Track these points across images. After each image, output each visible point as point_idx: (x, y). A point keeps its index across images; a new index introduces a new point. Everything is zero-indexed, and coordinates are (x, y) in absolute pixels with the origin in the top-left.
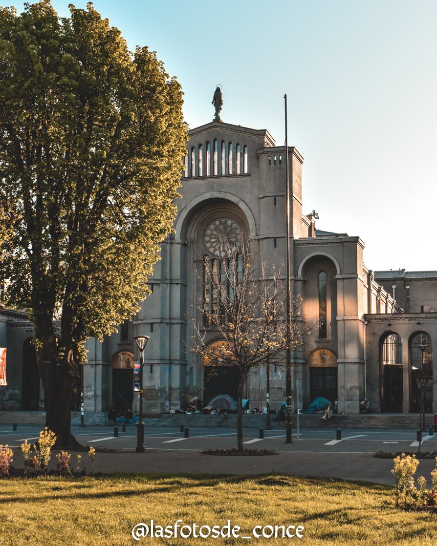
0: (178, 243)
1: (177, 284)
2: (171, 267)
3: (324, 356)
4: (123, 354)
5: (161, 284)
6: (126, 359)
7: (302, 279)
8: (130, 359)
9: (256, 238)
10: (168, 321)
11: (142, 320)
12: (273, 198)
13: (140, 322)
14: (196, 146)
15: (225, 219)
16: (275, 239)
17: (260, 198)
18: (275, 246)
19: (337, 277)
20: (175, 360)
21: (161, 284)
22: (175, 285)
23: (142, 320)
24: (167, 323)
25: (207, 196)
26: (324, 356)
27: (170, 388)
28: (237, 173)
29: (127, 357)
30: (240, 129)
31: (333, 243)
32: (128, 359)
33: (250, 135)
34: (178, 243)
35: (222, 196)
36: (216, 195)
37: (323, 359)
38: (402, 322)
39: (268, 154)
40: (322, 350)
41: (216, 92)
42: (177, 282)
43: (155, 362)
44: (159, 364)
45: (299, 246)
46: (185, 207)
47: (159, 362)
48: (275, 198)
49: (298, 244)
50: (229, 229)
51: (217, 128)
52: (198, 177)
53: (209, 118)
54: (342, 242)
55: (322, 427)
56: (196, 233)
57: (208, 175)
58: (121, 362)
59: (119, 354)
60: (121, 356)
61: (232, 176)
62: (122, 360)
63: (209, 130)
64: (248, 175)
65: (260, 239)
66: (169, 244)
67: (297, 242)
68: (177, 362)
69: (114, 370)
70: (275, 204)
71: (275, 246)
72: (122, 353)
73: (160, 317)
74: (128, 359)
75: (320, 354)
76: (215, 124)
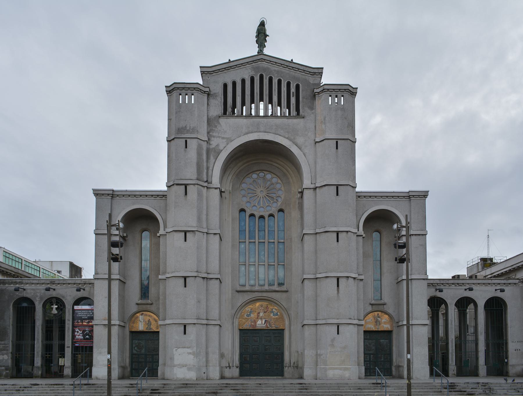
0: (216, 188)
2: (207, 215)
3: (379, 319)
4: (142, 314)
6: (147, 320)
8: (151, 320)
9: (313, 186)
10: (205, 275)
12: (335, 141)
15: (264, 172)
16: (337, 186)
17: (316, 142)
18: (337, 195)
21: (196, 232)
22: (212, 235)
24: (204, 278)
26: (379, 319)
29: (148, 318)
32: (149, 321)
33: (303, 74)
34: (216, 188)
38: (448, 287)
40: (376, 313)
41: (259, 26)
48: (337, 142)
49: (359, 196)
50: (269, 183)
53: (253, 50)
55: (239, 378)
56: (231, 184)
58: (140, 324)
59: (138, 315)
60: (140, 316)
62: (141, 322)
63: (254, 64)
65: (317, 187)
69: (132, 332)
70: (337, 148)
71: (337, 195)
72: (141, 313)
73: (196, 270)
74: (149, 321)
75: (374, 317)
76: (259, 57)
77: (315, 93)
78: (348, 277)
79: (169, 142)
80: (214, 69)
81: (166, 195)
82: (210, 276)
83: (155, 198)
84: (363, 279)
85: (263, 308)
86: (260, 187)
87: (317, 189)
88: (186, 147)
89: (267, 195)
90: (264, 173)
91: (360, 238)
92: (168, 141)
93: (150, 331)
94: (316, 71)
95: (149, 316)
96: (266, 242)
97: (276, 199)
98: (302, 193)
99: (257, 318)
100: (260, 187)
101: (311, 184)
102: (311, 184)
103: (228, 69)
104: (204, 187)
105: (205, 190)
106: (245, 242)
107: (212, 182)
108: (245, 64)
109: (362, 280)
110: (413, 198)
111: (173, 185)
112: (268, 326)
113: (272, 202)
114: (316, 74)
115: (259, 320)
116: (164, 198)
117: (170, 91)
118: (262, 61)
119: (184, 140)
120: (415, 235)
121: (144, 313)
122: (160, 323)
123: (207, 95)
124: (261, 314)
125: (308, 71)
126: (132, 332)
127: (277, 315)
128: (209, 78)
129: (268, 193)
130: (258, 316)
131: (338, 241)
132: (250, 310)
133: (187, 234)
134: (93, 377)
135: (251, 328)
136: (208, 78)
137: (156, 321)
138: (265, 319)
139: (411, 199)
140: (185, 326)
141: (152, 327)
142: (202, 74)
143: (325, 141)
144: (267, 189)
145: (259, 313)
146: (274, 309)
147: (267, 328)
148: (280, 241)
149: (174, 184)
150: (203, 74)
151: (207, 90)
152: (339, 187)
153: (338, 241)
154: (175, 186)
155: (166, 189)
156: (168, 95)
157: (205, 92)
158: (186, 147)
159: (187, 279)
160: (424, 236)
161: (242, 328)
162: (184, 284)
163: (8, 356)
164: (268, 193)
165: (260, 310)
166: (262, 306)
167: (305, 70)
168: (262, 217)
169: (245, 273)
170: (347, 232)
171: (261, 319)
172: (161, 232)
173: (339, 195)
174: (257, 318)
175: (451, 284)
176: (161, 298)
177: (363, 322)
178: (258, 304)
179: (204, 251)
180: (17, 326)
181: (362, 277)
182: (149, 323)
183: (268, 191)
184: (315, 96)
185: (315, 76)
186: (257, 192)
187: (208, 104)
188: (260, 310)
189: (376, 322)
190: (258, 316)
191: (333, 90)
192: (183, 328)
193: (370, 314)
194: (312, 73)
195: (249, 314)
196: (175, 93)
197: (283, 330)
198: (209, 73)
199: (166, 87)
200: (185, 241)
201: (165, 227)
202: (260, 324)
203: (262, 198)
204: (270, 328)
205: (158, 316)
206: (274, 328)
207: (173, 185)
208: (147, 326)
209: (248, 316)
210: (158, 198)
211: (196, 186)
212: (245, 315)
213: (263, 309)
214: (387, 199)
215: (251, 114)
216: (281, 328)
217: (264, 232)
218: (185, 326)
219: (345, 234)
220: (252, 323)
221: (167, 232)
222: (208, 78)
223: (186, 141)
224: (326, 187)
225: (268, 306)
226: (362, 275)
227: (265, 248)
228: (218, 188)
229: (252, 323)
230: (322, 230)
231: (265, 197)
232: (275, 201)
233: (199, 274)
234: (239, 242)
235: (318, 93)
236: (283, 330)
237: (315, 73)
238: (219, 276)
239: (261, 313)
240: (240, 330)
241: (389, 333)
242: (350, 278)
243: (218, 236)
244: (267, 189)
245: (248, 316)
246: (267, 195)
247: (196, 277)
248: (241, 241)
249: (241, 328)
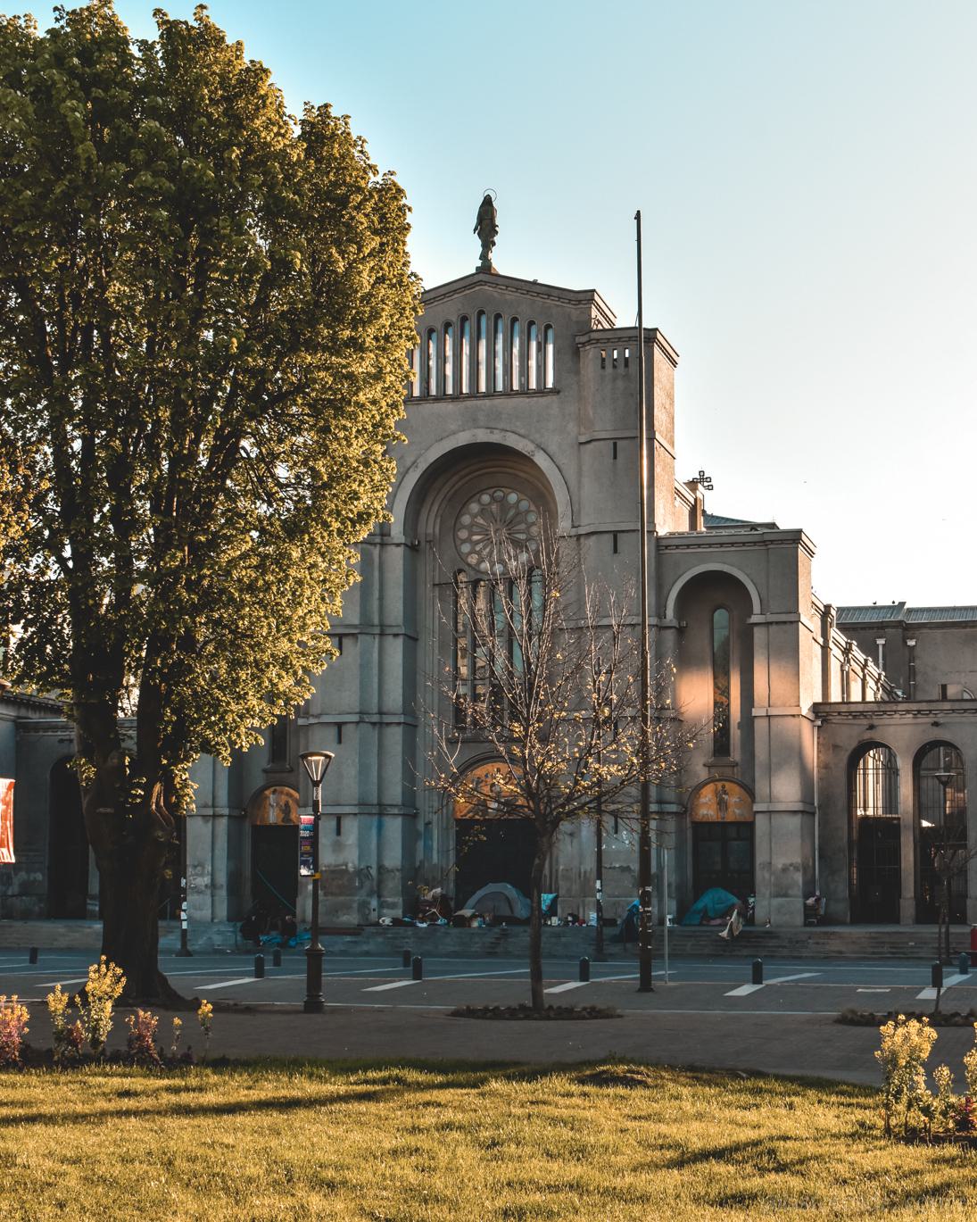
0: (398, 545)
2: (381, 598)
3: (726, 797)
6: (282, 803)
7: (675, 623)
8: (291, 802)
9: (573, 532)
10: (375, 719)
13: (312, 721)
14: (439, 326)
16: (615, 534)
17: (581, 443)
18: (615, 551)
19: (754, 619)
24: (374, 724)
25: (463, 439)
26: (726, 797)
27: (381, 868)
32: (287, 804)
34: (398, 545)
35: (495, 438)
36: (482, 436)
37: (722, 805)
40: (720, 785)
42: (395, 631)
43: (347, 810)
45: (668, 551)
48: (615, 444)
49: (667, 547)
51: (486, 288)
52: (442, 397)
59: (267, 792)
64: (555, 391)
67: (664, 543)
70: (615, 457)
71: (615, 551)
72: (272, 789)
74: (287, 804)
75: (716, 793)
94: (581, 297)
120: (777, 623)
121: (277, 788)
126: (256, 829)
159: (344, 729)
160: (794, 625)
163: (43, 875)
176: (735, 733)
179: (375, 671)
180: (273, 750)
189: (719, 804)
214: (733, 549)
215: (461, 393)
235: (583, 344)
237: (580, 301)
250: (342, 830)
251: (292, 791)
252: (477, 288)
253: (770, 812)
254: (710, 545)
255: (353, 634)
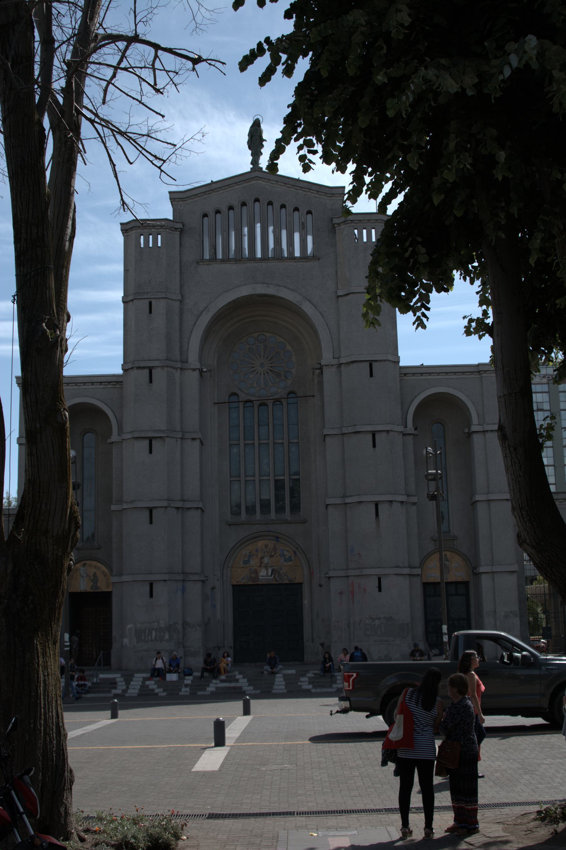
0: (194, 370)
1: (193, 439)
2: (181, 411)
5: (167, 439)
7: (413, 431)
9: (335, 362)
10: (179, 504)
11: (132, 502)
13: (125, 506)
14: (224, 209)
18: (371, 375)
19: (474, 428)
20: (191, 574)
21: (167, 439)
23: (132, 502)
24: (178, 508)
25: (245, 291)
27: (185, 624)
28: (205, 258)
30: (214, 186)
31: (101, 383)
32: (95, 575)
33: (317, 195)
34: (194, 370)
35: (271, 291)
36: (261, 289)
37: (443, 569)
39: (353, 224)
42: (193, 436)
43: (158, 577)
44: (165, 581)
45: (405, 378)
46: (206, 308)
47: (166, 577)
49: (405, 374)
51: (261, 182)
52: (226, 260)
54: (479, 372)
57: (270, 256)
60: (82, 568)
61: (287, 259)
62: (83, 577)
63: (245, 184)
64: (315, 257)
66: (179, 370)
67: (404, 371)
68: (196, 578)
71: (371, 375)
72: (83, 563)
74: (95, 575)
77: (334, 224)
78: (391, 502)
79: (126, 304)
80: (188, 194)
81: (122, 382)
82: (188, 505)
83: (105, 387)
84: (416, 503)
85: (268, 550)
86: (260, 357)
87: (343, 366)
88: (150, 312)
89: (270, 370)
90: (265, 336)
91: (410, 439)
92: (124, 302)
93: (96, 591)
95: (95, 567)
96: (270, 444)
97: (284, 376)
98: (321, 369)
99: (260, 566)
100: (260, 357)
101: (334, 358)
102: (334, 358)
103: (210, 194)
104: (176, 369)
105: (177, 374)
106: (239, 444)
107: (187, 359)
108: (232, 185)
109: (414, 504)
110: (485, 375)
111: (132, 368)
112: (278, 578)
113: (278, 380)
114: (336, 195)
115: (263, 570)
116: (117, 386)
117: (126, 230)
118: (257, 180)
119: (147, 302)
122: (115, 579)
123: (179, 233)
124: (266, 560)
125: (323, 191)
127: (291, 560)
128: (182, 207)
129: (271, 367)
130: (261, 563)
131: (374, 446)
132: (248, 554)
133: (154, 442)
134: (467, 580)
135: (250, 583)
136: (181, 207)
137: (105, 575)
138: (272, 567)
139: (483, 375)
140: (151, 585)
141: (99, 585)
142: (171, 202)
143: (350, 296)
144: (270, 360)
145: (262, 558)
146: (285, 552)
147: (275, 583)
148: (292, 441)
149: (134, 367)
150: (173, 201)
151: (179, 226)
152: (373, 364)
153: (374, 446)
154: (135, 371)
155: (121, 372)
156: (124, 235)
157: (176, 229)
158: (150, 312)
159: (154, 512)
161: (237, 582)
162: (148, 519)
164: (271, 367)
165: (264, 552)
166: (266, 546)
167: (318, 190)
168: (263, 404)
169: (239, 494)
170: (388, 432)
171: (266, 567)
172: (115, 437)
173: (374, 375)
174: (260, 566)
175: (563, 500)
177: (418, 571)
178: (260, 544)
181: (414, 499)
182: (95, 579)
183: (271, 363)
184: (334, 227)
185: (334, 198)
186: (254, 366)
187: (181, 245)
188: (264, 552)
190: (261, 563)
191: (359, 222)
192: (148, 588)
193: (433, 556)
194: (329, 194)
195: (246, 559)
196: (133, 233)
197: (301, 584)
198: (183, 200)
199: (121, 224)
200: (151, 452)
201: (121, 431)
202: (264, 575)
203: (262, 374)
204: (280, 582)
205: (110, 569)
206: (286, 582)
207: (132, 368)
208: (92, 583)
209: (246, 562)
210: (109, 386)
211: (166, 369)
212: (241, 563)
213: (269, 552)
216: (297, 581)
217: (267, 427)
218: (151, 585)
219: (384, 434)
220: (252, 575)
221: (123, 440)
222: (181, 207)
223: (150, 303)
224: (355, 365)
225: (275, 547)
226: (414, 496)
227: (269, 453)
228: (197, 369)
229: (252, 575)
230: (351, 430)
231: (268, 373)
232: (283, 378)
233: (171, 502)
234: (230, 445)
235: (339, 224)
236: (301, 584)
238: (200, 505)
239: (265, 558)
240: (234, 586)
241: (466, 584)
242: (394, 503)
243: (198, 442)
244: (270, 360)
245: (246, 562)
246: (270, 370)
247: (166, 507)
248: (232, 443)
249: (235, 583)
250: (154, 593)
251: (99, 565)
252: (253, 182)
253: (493, 572)
254: (439, 374)
255: (161, 437)
